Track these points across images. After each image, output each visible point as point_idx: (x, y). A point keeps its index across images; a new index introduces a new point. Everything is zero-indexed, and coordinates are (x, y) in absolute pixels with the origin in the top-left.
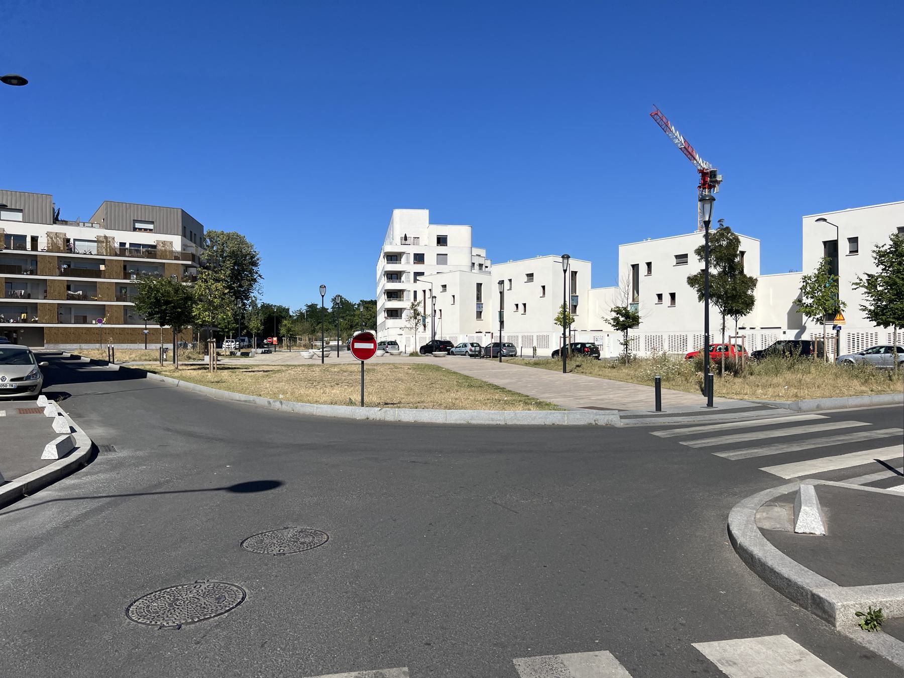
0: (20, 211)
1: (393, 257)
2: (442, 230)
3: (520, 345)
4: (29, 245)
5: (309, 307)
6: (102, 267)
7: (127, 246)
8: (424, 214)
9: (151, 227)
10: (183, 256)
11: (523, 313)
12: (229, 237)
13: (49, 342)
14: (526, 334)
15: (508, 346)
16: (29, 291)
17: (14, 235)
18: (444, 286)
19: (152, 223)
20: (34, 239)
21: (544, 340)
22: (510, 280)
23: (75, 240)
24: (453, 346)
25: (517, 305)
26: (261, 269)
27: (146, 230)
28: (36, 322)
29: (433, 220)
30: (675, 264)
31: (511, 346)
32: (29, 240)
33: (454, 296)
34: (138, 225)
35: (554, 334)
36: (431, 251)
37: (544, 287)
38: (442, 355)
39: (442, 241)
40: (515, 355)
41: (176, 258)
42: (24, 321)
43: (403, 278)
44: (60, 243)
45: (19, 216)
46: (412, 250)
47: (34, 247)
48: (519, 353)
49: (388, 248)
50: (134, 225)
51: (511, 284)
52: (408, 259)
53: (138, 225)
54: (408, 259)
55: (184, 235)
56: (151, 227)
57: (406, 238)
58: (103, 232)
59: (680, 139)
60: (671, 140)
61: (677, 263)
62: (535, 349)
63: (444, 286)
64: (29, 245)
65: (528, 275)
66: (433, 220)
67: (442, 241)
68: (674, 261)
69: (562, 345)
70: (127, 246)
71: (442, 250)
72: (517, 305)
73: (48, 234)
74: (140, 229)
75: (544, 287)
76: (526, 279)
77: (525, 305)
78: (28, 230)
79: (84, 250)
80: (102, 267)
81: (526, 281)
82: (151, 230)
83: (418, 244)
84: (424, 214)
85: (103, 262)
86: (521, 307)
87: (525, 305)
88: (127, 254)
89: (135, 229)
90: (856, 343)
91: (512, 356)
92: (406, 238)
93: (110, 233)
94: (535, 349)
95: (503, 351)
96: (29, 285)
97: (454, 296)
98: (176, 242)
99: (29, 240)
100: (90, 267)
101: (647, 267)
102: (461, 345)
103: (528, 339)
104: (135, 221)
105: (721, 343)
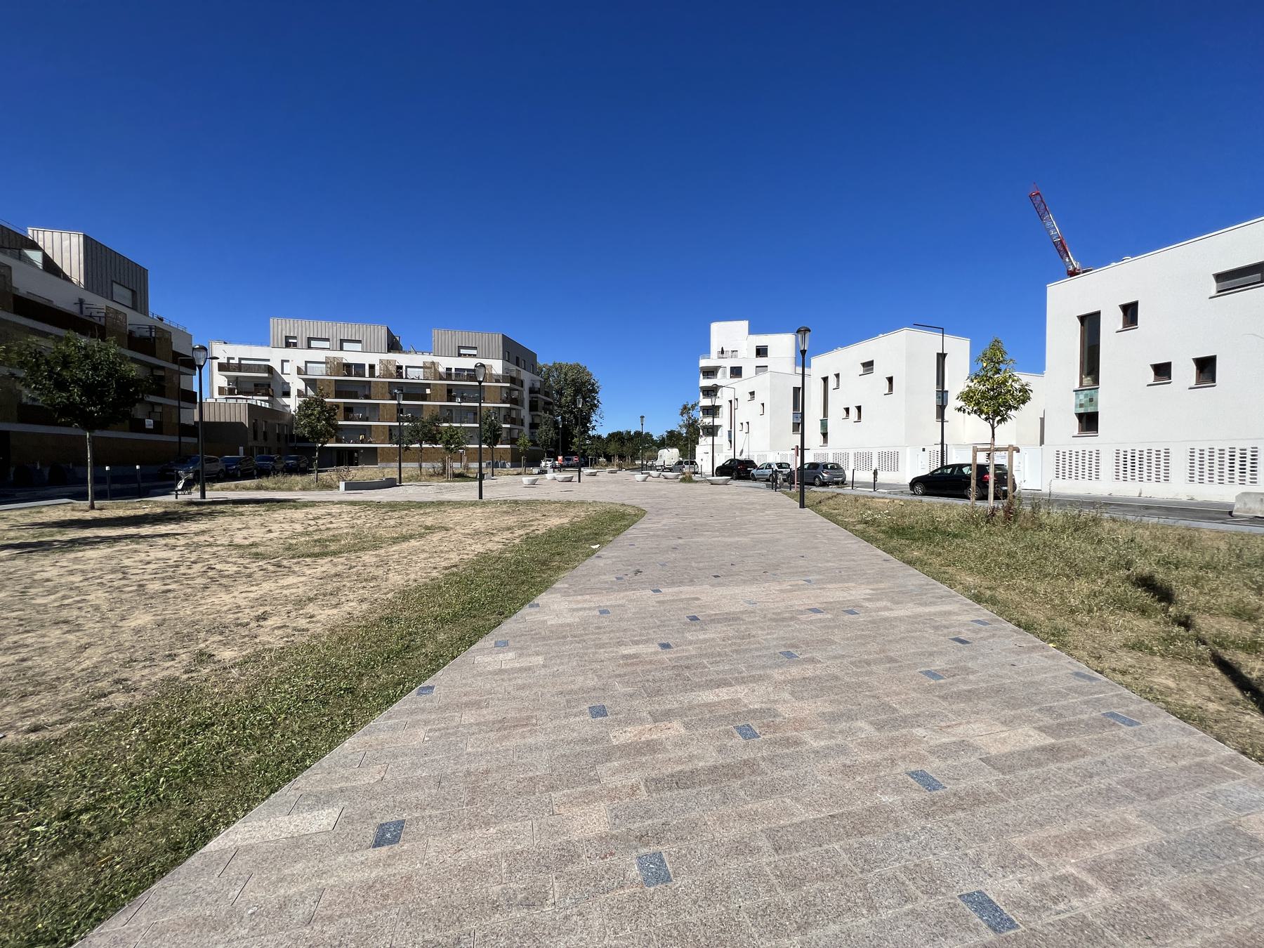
0: (359, 342)
1: (710, 372)
2: (762, 340)
3: (852, 467)
4: (367, 374)
5: (669, 432)
6: (428, 391)
7: (453, 371)
8: (744, 325)
9: (474, 352)
10: (505, 379)
11: (856, 419)
12: (572, 368)
13: (382, 461)
14: (860, 451)
15: (832, 468)
16: (367, 415)
17: (355, 365)
18: (752, 393)
19: (475, 348)
20: (372, 367)
21: (891, 460)
22: (837, 376)
23: (407, 367)
24: (755, 466)
25: (847, 410)
26: (601, 396)
27: (470, 355)
28: (370, 443)
29: (753, 330)
30: (1214, 292)
31: (836, 468)
32: (367, 367)
33: (763, 404)
34: (463, 351)
35: (908, 450)
36: (748, 361)
37: (890, 380)
38: (721, 482)
39: (761, 352)
40: (843, 482)
41: (497, 381)
42: (362, 442)
43: (719, 394)
44: (393, 369)
45: (358, 347)
46: (728, 363)
47: (372, 374)
48: (849, 478)
49: (704, 363)
50: (459, 351)
51: (838, 381)
52: (724, 373)
53: (463, 351)
54: (724, 373)
55: (504, 359)
56: (474, 352)
57: (722, 352)
58: (428, 358)
59: (1056, 231)
60: (1048, 230)
61: (1219, 292)
62: (875, 473)
63: (752, 393)
64: (367, 374)
65: (864, 365)
66: (753, 330)
67: (761, 352)
68: (1213, 287)
69: (799, 465)
70: (453, 371)
71: (762, 361)
72: (847, 410)
73: (381, 361)
74: (465, 355)
75: (890, 380)
76: (861, 370)
77: (859, 408)
78: (367, 359)
79: (415, 376)
80: (428, 391)
81: (862, 373)
82: (475, 355)
83: (736, 357)
84: (744, 325)
85: (428, 386)
86: (853, 412)
87: (859, 408)
88: (453, 378)
89: (460, 355)
90: (1087, 466)
91: (837, 483)
92: (722, 352)
93: (436, 359)
94: (875, 473)
95: (823, 476)
96: (367, 409)
97: (763, 404)
98: (497, 366)
99: (367, 367)
100: (416, 391)
101: (1122, 314)
102: (765, 466)
103: (863, 458)
104: (460, 348)
105: (970, 461)
